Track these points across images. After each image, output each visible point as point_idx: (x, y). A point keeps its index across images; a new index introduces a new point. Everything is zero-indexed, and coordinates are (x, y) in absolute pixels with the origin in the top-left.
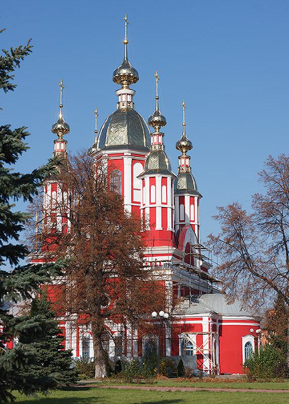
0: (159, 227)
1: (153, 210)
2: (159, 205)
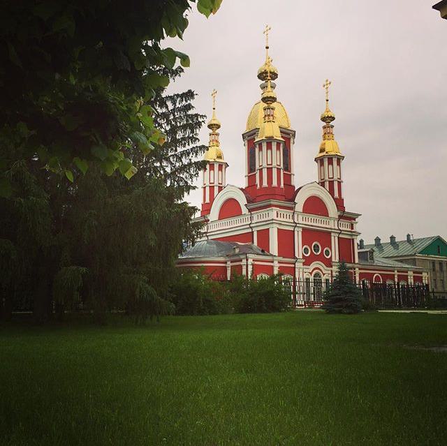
0: (275, 183)
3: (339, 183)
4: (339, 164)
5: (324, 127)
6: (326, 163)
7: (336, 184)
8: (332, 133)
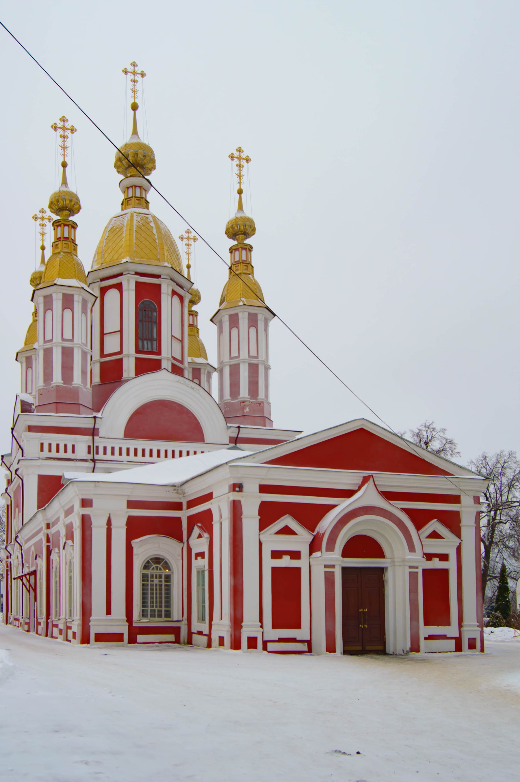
1: (48, 353)
2: (244, 355)
3: (254, 369)
4: (253, 321)
6: (243, 322)
8: (73, 241)
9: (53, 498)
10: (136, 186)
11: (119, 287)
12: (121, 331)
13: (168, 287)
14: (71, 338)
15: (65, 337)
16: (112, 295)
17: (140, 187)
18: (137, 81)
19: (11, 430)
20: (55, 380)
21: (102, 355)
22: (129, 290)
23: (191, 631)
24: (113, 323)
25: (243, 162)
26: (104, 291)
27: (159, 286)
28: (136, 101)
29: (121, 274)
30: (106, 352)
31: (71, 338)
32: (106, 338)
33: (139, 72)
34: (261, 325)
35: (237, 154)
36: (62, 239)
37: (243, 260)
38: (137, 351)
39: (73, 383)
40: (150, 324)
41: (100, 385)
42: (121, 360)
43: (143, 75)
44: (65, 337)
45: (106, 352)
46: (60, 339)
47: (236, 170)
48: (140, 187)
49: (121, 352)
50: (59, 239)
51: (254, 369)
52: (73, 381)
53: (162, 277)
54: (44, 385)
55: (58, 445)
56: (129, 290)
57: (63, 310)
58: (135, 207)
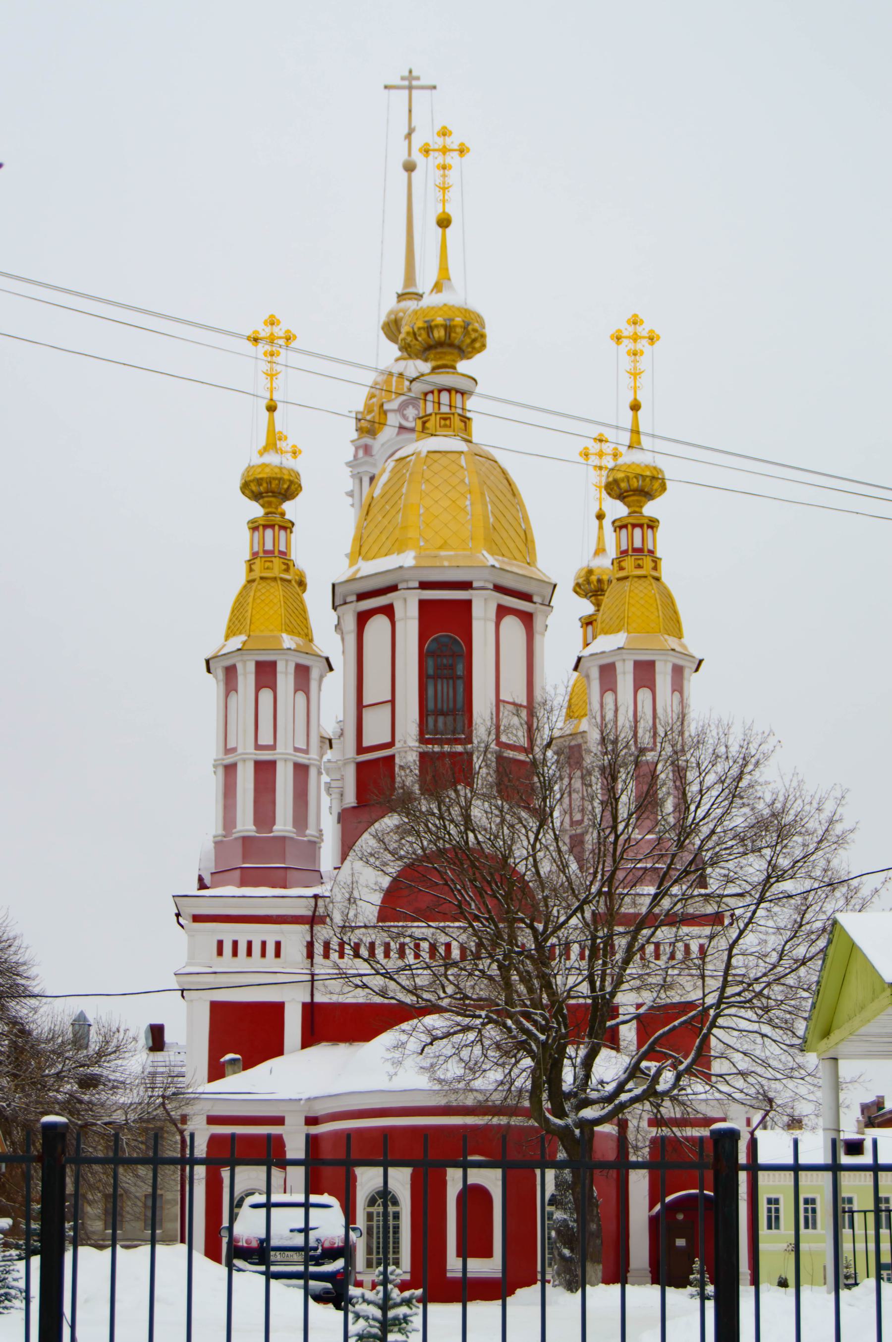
5: (254, 526)
7: (284, 779)
9: (470, 1120)
10: (457, 391)
11: (388, 611)
12: (393, 701)
13: (485, 604)
14: (271, 743)
15: (260, 742)
16: (378, 626)
17: (449, 391)
18: (450, 167)
19: (175, 918)
20: (239, 827)
21: (361, 749)
22: (485, 619)
23: (471, 1300)
24: (378, 689)
25: (642, 344)
26: (363, 618)
27: (468, 603)
28: (448, 210)
29: (393, 588)
30: (366, 743)
31: (271, 743)
32: (367, 714)
33: (455, 146)
34: (313, 685)
35: (628, 330)
36: (261, 554)
37: (265, 552)
38: (422, 740)
39: (275, 828)
40: (451, 682)
41: (354, 807)
42: (392, 757)
43: (462, 151)
44: (261, 742)
45: (366, 743)
46: (251, 748)
47: (626, 363)
48: (449, 391)
49: (391, 744)
50: (255, 555)
51: (361, 597)
52: (274, 823)
53: (475, 585)
54: (224, 833)
55: (250, 944)
56: (406, 618)
57: (295, 692)
58: (438, 433)
